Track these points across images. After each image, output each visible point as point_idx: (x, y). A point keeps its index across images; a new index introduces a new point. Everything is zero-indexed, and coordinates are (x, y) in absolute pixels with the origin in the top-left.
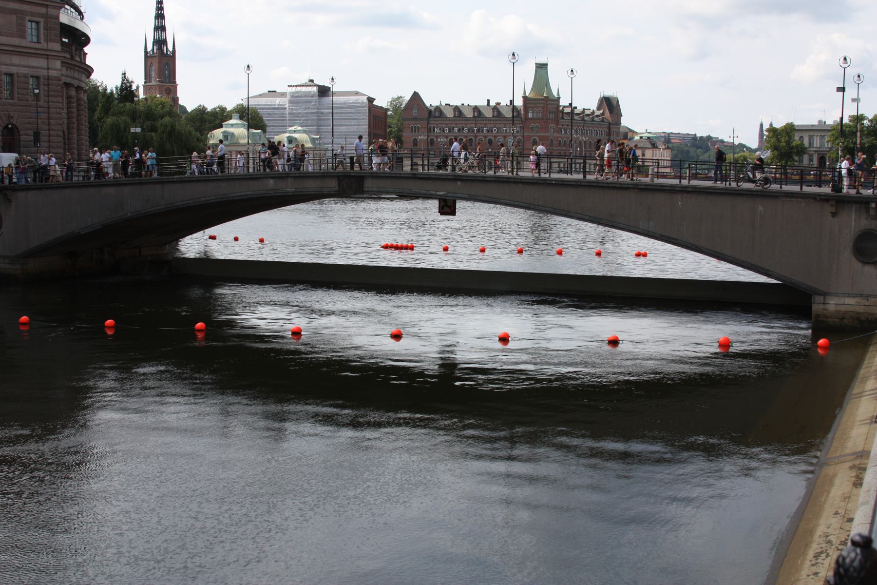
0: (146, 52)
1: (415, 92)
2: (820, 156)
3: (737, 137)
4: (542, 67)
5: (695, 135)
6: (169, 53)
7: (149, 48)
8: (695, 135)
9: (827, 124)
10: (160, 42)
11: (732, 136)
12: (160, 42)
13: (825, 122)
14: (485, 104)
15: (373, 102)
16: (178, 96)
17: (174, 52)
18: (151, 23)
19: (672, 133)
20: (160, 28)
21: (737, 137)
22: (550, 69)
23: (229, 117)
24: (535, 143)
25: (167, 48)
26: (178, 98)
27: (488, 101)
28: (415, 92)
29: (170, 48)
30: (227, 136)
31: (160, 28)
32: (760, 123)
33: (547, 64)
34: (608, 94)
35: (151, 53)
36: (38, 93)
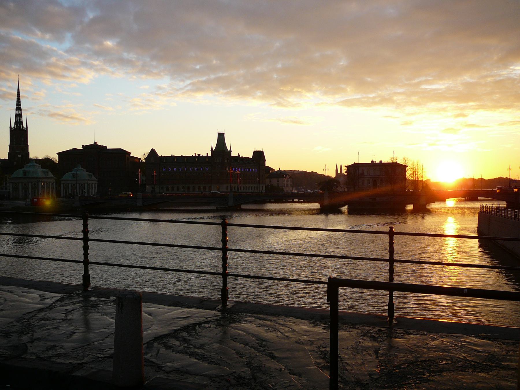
0: (11, 128)
1: (152, 149)
2: (374, 180)
3: (328, 170)
4: (221, 136)
5: (306, 171)
6: (24, 129)
7: (13, 126)
8: (306, 171)
9: (376, 162)
10: (19, 123)
11: (325, 170)
12: (19, 123)
13: (375, 161)
14: (206, 155)
15: (130, 154)
16: (29, 152)
17: (27, 128)
18: (14, 113)
19: (295, 170)
20: (19, 115)
21: (328, 170)
22: (225, 134)
23: (441, 197)
24: (407, 191)
25: (23, 126)
26: (29, 153)
27: (207, 154)
28: (152, 149)
29: (25, 126)
30: (26, 173)
31: (19, 115)
32: (340, 164)
33: (224, 133)
34: (259, 149)
35: (14, 128)
36: (285, 175)
